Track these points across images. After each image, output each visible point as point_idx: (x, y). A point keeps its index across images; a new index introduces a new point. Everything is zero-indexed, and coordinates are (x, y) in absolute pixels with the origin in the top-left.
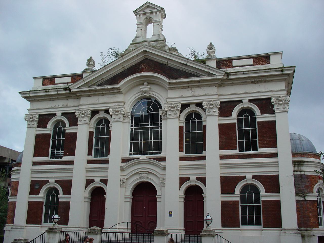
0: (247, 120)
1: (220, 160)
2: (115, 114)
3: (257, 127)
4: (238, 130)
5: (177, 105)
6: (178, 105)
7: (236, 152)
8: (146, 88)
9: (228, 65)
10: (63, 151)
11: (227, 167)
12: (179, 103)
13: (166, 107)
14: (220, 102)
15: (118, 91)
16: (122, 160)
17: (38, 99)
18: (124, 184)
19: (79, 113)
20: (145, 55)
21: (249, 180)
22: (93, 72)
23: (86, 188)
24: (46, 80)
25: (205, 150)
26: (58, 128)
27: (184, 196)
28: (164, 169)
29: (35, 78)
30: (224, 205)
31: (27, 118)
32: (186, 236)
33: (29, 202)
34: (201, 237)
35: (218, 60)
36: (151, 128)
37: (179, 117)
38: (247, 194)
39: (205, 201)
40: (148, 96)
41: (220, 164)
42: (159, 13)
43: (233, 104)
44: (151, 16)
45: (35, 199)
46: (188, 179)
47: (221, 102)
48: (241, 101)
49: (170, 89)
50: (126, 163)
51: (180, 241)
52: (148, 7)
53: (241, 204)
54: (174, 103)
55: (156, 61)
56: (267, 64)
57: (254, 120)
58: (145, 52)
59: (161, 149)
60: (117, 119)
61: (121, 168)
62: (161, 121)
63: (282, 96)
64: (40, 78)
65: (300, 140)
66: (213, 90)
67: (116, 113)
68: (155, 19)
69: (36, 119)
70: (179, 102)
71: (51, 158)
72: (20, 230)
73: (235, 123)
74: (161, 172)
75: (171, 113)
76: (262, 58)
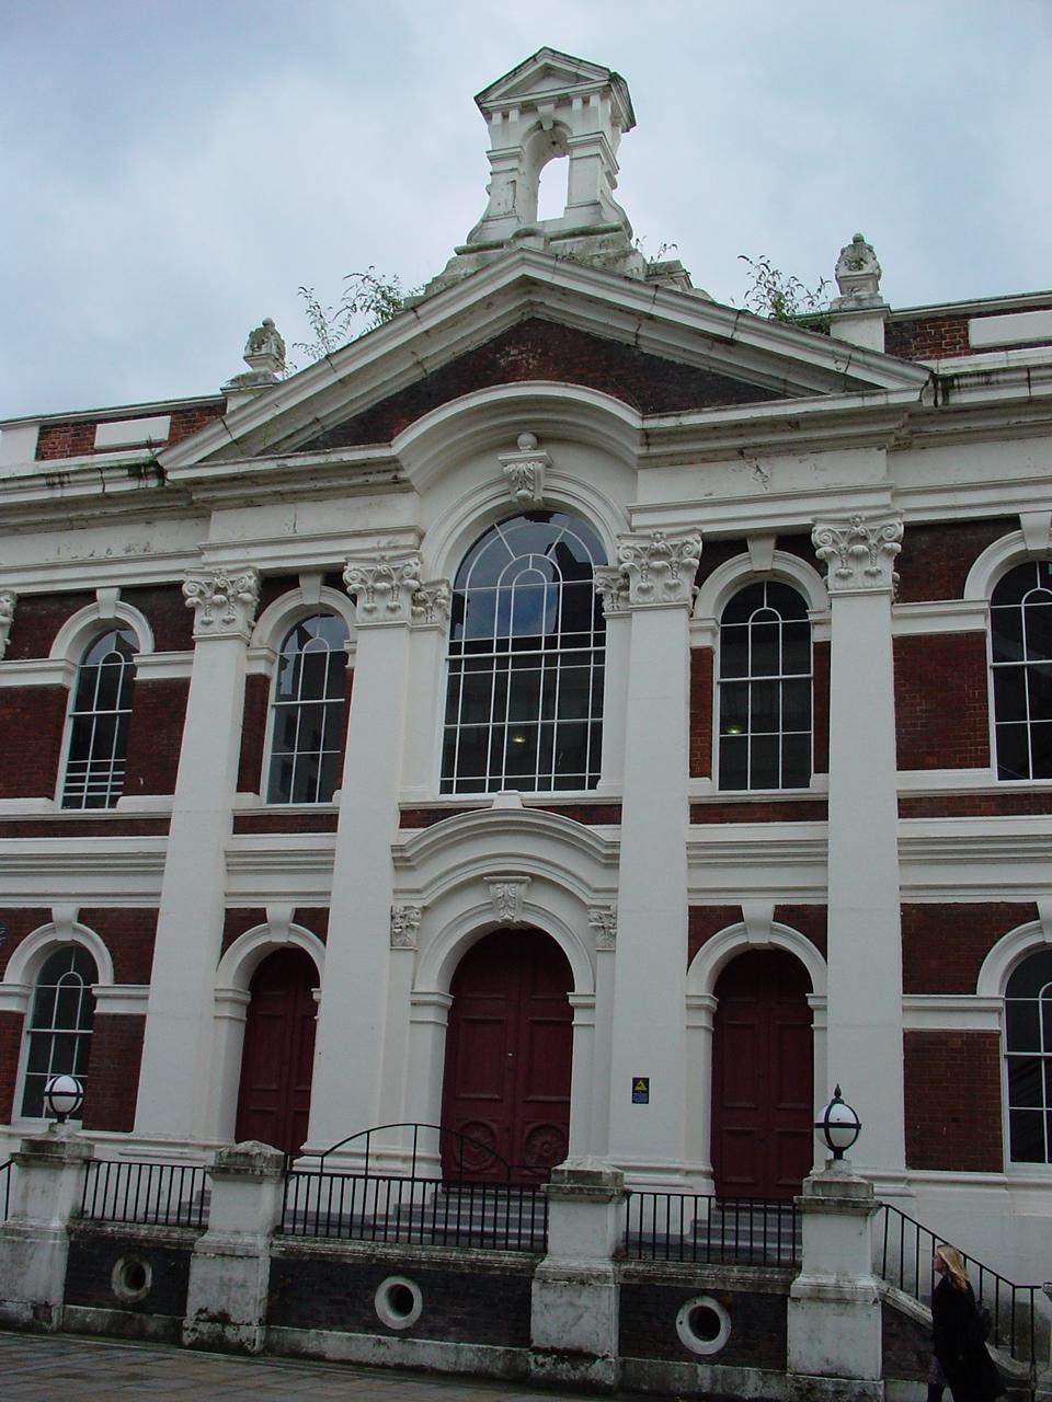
1: (901, 820)
2: (375, 591)
4: (722, 684)
7: (984, 778)
8: (529, 460)
13: (628, 552)
14: (905, 527)
15: (392, 479)
19: (199, 587)
20: (525, 299)
23: (224, 949)
25: (823, 767)
26: (1026, 602)
28: (611, 862)
30: (921, 1051)
32: (717, 1207)
34: (797, 1212)
40: (535, 500)
41: (902, 842)
44: (562, 116)
47: (911, 529)
48: (1012, 522)
49: (648, 462)
52: (548, 72)
53: (1009, 1050)
54: (866, 514)
59: (596, 766)
60: (381, 615)
61: (399, 854)
62: (601, 624)
66: (868, 467)
67: (380, 585)
71: (67, 803)
73: (983, 634)
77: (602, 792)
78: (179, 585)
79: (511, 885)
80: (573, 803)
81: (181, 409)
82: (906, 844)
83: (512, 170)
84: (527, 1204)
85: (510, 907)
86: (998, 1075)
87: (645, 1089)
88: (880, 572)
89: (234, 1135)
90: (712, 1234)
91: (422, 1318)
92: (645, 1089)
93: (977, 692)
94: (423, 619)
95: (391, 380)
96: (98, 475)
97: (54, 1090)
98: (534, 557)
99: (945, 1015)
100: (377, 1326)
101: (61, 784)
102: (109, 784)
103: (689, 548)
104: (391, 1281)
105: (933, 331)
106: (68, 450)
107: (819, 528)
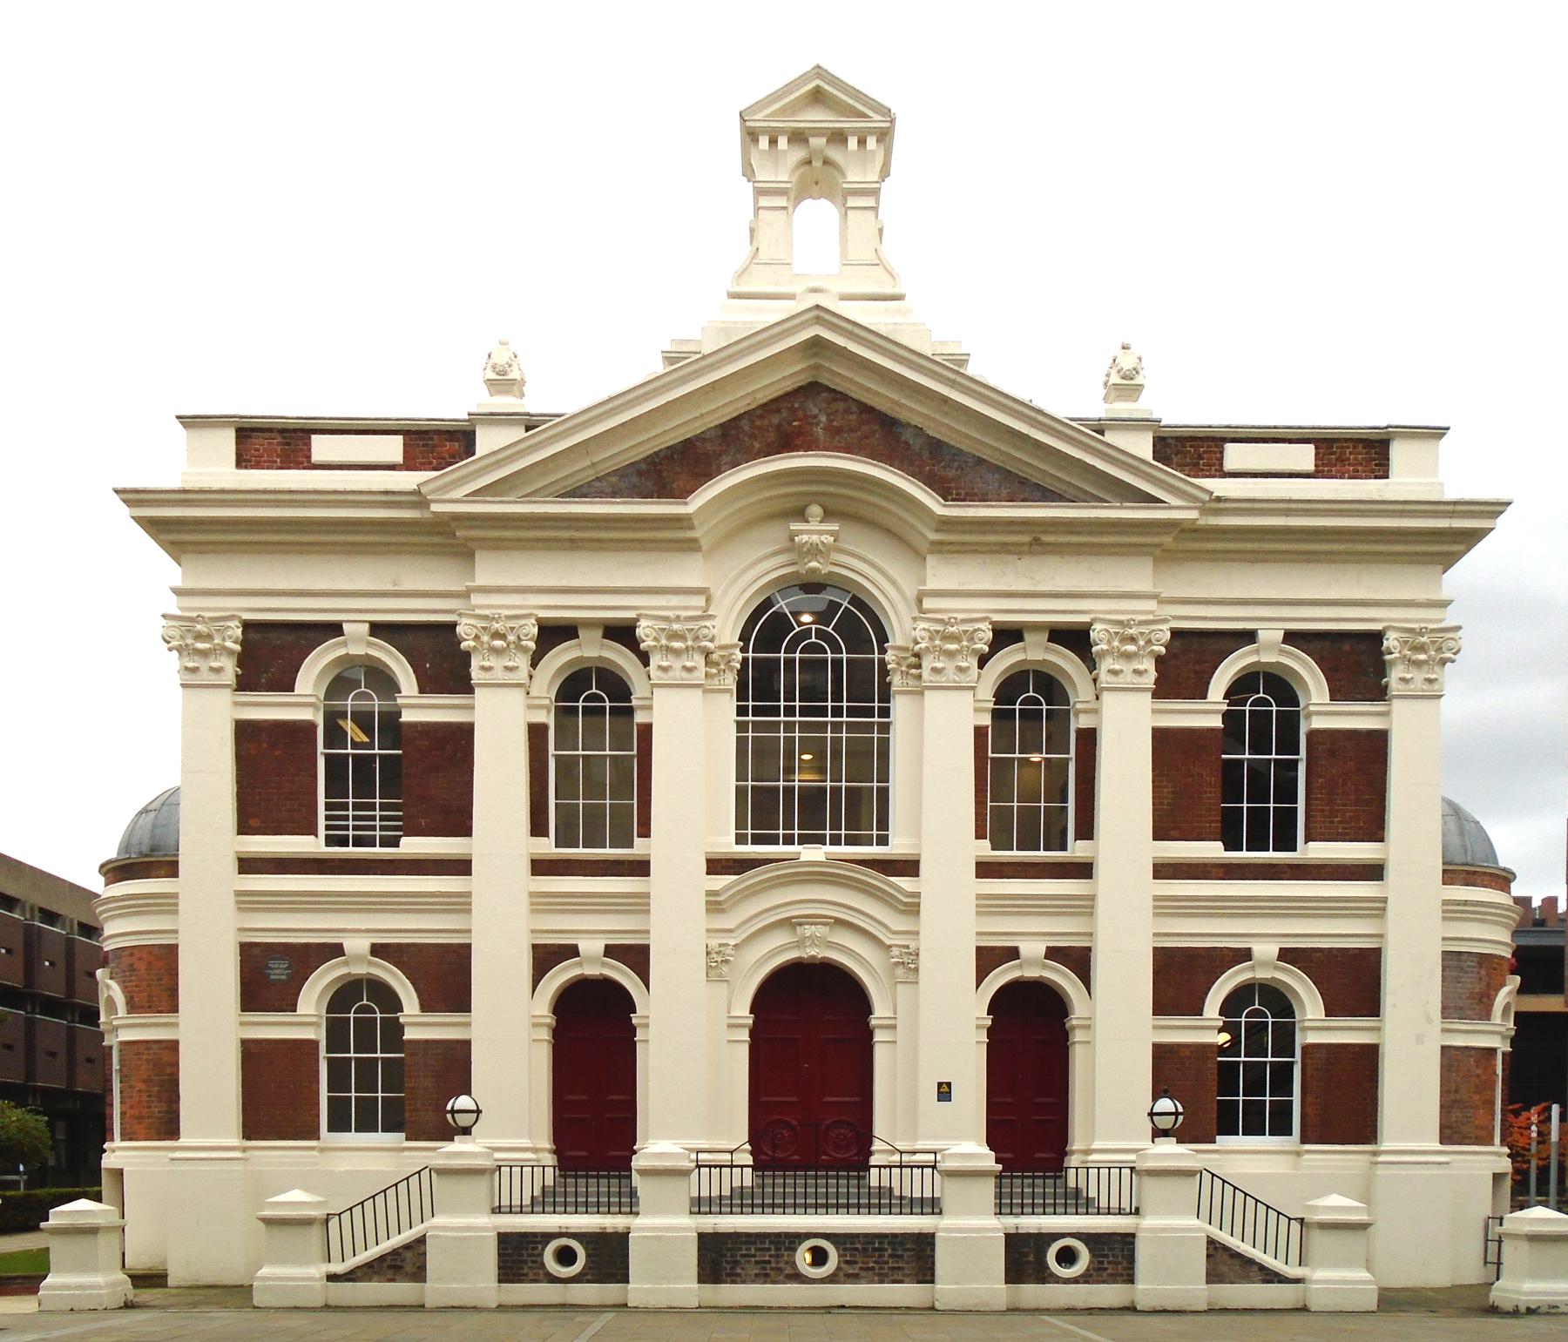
2: (669, 650)
4: (557, 757)
5: (971, 629)
6: (521, 627)
8: (820, 533)
10: (401, 813)
14: (1171, 632)
16: (709, 861)
18: (725, 969)
19: (475, 631)
20: (812, 362)
23: (977, 988)
24: (258, 437)
25: (645, 832)
27: (550, 1020)
29: (190, 422)
30: (255, 1056)
32: (560, 1176)
35: (1162, 435)
37: (528, 678)
38: (1243, 1019)
41: (1445, 902)
43: (1215, 645)
44: (834, 154)
45: (272, 1028)
46: (572, 951)
47: (1176, 633)
48: (1249, 637)
49: (939, 548)
50: (737, 877)
52: (817, 97)
54: (961, 616)
56: (1376, 477)
57: (1290, 723)
58: (815, 350)
59: (883, 823)
60: (677, 675)
62: (886, 697)
63: (1431, 626)
64: (1145, 428)
65: (1460, 818)
66: (1136, 576)
67: (200, 646)
69: (229, 644)
71: (330, 841)
74: (896, 922)
75: (196, 665)
76: (1355, 448)
77: (898, 846)
79: (818, 926)
80: (1246, 861)
82: (983, 899)
84: (1017, 1182)
85: (816, 945)
87: (948, 1090)
88: (1146, 670)
91: (838, 1268)
92: (948, 1090)
93: (1213, 779)
97: (1154, 1111)
98: (816, 629)
100: (798, 1277)
101: (322, 823)
103: (981, 635)
105: (1192, 450)
107: (643, 623)
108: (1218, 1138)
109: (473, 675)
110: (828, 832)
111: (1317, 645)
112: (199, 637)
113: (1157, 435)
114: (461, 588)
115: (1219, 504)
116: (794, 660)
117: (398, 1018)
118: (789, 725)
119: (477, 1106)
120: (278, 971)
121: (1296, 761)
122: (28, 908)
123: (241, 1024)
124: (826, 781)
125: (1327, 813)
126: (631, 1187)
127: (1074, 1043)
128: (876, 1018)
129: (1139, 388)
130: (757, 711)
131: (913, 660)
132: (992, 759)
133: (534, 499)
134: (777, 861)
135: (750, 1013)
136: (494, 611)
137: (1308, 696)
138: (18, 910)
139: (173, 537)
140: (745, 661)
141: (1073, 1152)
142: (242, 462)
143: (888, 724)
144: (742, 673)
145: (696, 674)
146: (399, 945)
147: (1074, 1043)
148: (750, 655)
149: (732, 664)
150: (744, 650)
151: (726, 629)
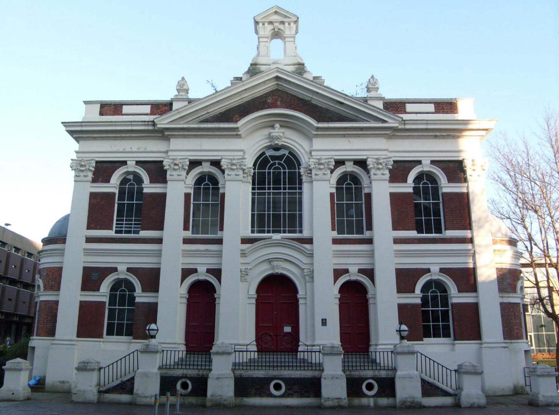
0: (349, 189)
3: (364, 201)
7: (110, 233)
9: (400, 110)
11: (402, 255)
12: (93, 160)
15: (235, 134)
16: (242, 239)
17: (123, 135)
19: (169, 163)
21: (435, 274)
22: (190, 101)
23: (335, 283)
28: (311, 256)
30: (84, 306)
31: (75, 165)
33: (81, 302)
36: (285, 194)
38: (118, 293)
39: (217, 303)
42: (294, 24)
43: (117, 165)
45: (91, 297)
46: (195, 271)
47: (395, 162)
49: (316, 136)
50: (250, 245)
51: (248, 361)
52: (276, 13)
55: (292, 95)
59: (301, 225)
61: (243, 252)
62: (301, 183)
67: (82, 169)
68: (287, 33)
70: (331, 157)
71: (117, 232)
72: (67, 346)
76: (446, 105)
77: (306, 234)
78: (162, 162)
81: (154, 103)
83: (266, 41)
86: (104, 313)
89: (184, 339)
90: (286, 362)
91: (285, 392)
94: (246, 179)
95: (233, 103)
96: (426, 122)
98: (278, 162)
99: (404, 299)
100: (271, 395)
101: (114, 225)
102: (133, 226)
104: (184, 380)
106: (112, 113)
107: (223, 160)
108: (424, 339)
109: (168, 177)
110: (282, 229)
111: (441, 165)
112: (82, 166)
113: (384, 102)
114: (165, 150)
115: (404, 122)
116: (271, 172)
117: (134, 294)
118: (269, 192)
119: (158, 328)
120: (95, 276)
121: (439, 203)
122: (36, 257)
123: (248, 298)
124: (265, 212)
125: (451, 220)
126: (376, 363)
127: (370, 304)
128: (137, 293)
129: (378, 88)
130: (259, 189)
131: (309, 172)
132: (336, 203)
133: (173, 123)
134: (264, 239)
135: (339, 293)
136: (175, 157)
137: (441, 182)
138: (33, 258)
139: (77, 136)
140: (254, 173)
141: (372, 345)
142: (101, 114)
143: (302, 192)
144: (254, 177)
145: (240, 176)
146: (136, 268)
147: (370, 304)
148: (256, 171)
149: (251, 174)
150: (254, 169)
151: (249, 162)
